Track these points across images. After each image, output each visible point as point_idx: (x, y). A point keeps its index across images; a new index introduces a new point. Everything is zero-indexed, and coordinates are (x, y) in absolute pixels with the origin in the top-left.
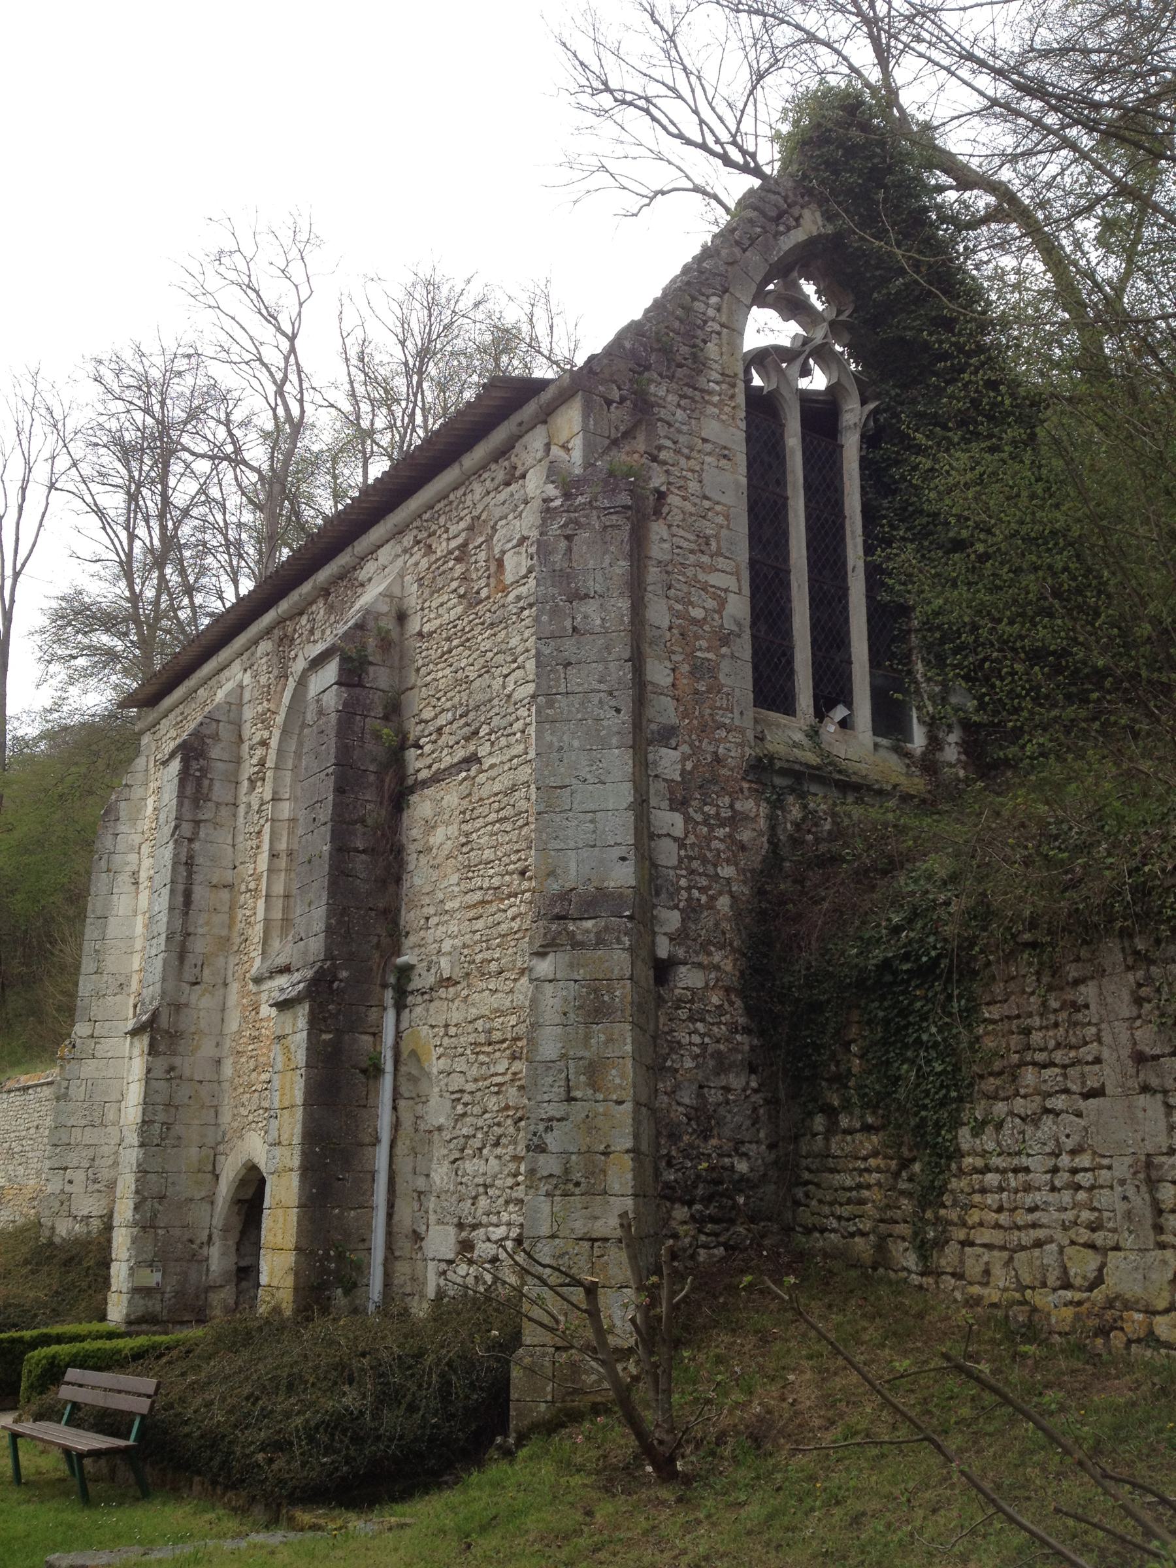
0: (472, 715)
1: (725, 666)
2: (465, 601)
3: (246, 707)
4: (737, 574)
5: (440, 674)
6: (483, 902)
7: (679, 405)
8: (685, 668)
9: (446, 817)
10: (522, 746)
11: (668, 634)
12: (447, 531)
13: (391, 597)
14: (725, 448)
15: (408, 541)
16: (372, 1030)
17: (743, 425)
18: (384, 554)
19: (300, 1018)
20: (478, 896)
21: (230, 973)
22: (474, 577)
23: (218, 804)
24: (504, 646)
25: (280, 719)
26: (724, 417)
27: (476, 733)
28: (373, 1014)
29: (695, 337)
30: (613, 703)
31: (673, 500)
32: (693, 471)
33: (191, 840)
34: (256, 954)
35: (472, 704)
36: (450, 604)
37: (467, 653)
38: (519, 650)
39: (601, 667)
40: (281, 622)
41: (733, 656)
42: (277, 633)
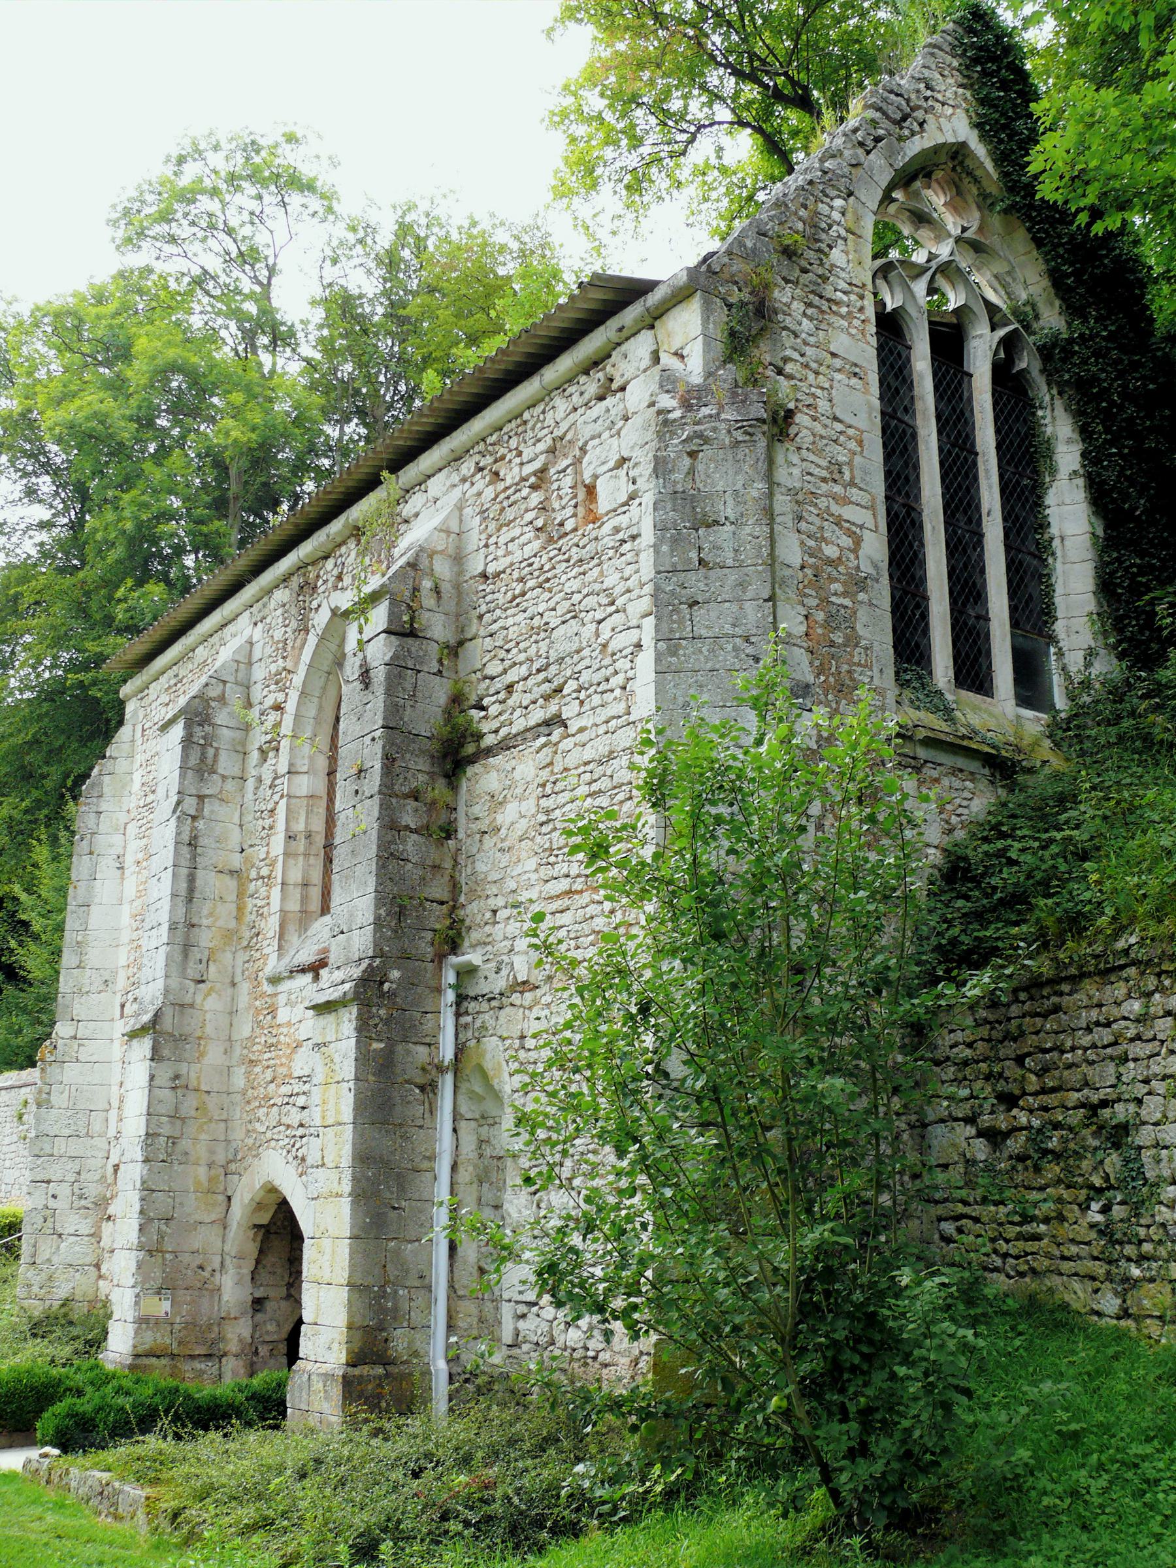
0: (553, 669)
1: (863, 615)
2: (543, 536)
3: (255, 666)
4: (872, 508)
5: (510, 621)
6: (570, 892)
7: (804, 314)
8: (820, 616)
9: (519, 791)
10: (623, 705)
11: (800, 574)
12: (520, 454)
13: (448, 532)
14: (856, 365)
15: (467, 467)
16: (427, 1040)
17: (874, 341)
18: (435, 486)
19: (346, 1023)
20: (564, 885)
21: (239, 971)
22: (556, 505)
23: (224, 777)
24: (597, 587)
25: (298, 679)
26: (854, 331)
27: (559, 690)
28: (429, 1022)
29: (818, 241)
30: (750, 650)
31: (801, 419)
32: (823, 389)
33: (194, 818)
34: (271, 949)
35: (553, 655)
36: (523, 539)
37: (547, 595)
38: (617, 591)
39: (734, 607)
40: (302, 567)
41: (871, 604)
42: (296, 581)
